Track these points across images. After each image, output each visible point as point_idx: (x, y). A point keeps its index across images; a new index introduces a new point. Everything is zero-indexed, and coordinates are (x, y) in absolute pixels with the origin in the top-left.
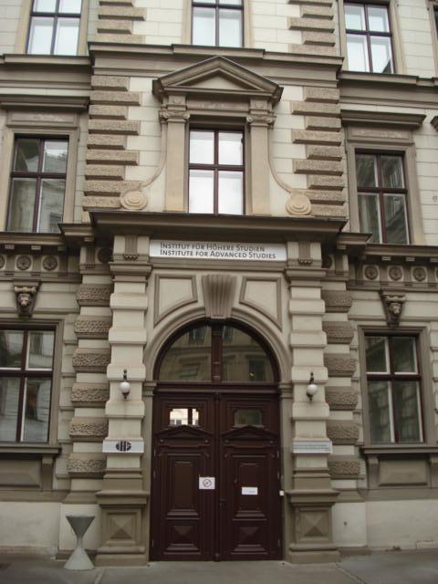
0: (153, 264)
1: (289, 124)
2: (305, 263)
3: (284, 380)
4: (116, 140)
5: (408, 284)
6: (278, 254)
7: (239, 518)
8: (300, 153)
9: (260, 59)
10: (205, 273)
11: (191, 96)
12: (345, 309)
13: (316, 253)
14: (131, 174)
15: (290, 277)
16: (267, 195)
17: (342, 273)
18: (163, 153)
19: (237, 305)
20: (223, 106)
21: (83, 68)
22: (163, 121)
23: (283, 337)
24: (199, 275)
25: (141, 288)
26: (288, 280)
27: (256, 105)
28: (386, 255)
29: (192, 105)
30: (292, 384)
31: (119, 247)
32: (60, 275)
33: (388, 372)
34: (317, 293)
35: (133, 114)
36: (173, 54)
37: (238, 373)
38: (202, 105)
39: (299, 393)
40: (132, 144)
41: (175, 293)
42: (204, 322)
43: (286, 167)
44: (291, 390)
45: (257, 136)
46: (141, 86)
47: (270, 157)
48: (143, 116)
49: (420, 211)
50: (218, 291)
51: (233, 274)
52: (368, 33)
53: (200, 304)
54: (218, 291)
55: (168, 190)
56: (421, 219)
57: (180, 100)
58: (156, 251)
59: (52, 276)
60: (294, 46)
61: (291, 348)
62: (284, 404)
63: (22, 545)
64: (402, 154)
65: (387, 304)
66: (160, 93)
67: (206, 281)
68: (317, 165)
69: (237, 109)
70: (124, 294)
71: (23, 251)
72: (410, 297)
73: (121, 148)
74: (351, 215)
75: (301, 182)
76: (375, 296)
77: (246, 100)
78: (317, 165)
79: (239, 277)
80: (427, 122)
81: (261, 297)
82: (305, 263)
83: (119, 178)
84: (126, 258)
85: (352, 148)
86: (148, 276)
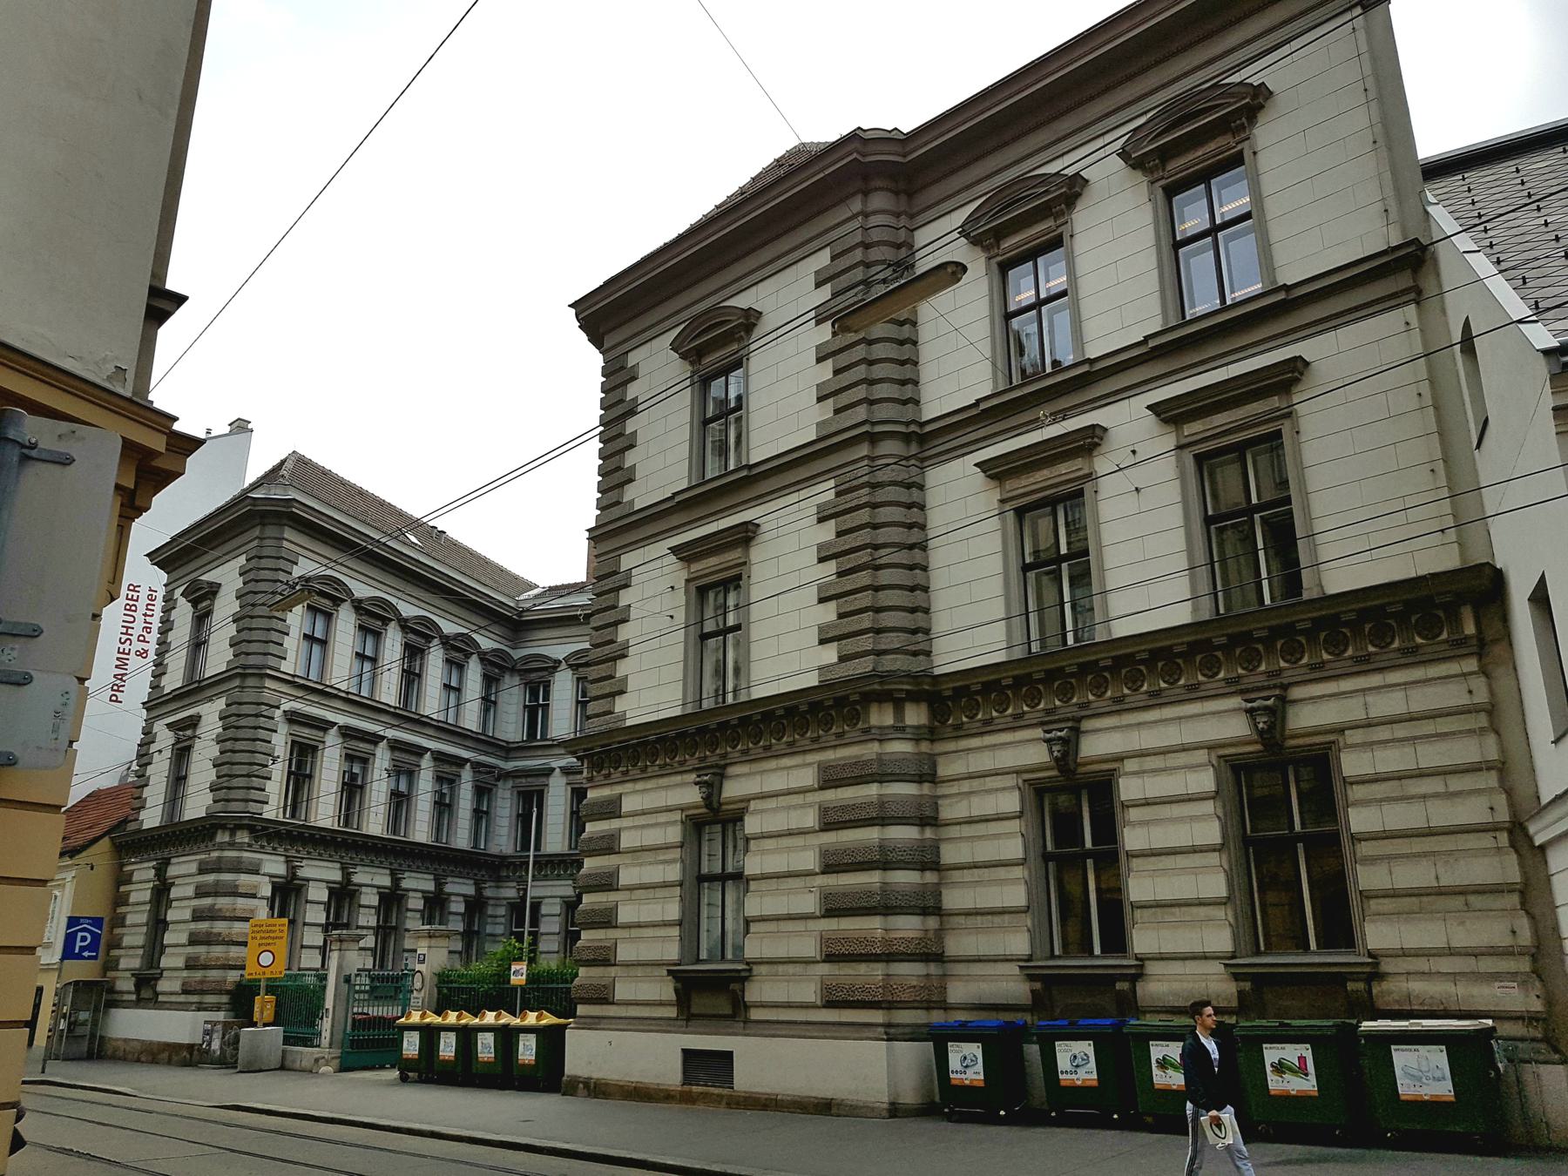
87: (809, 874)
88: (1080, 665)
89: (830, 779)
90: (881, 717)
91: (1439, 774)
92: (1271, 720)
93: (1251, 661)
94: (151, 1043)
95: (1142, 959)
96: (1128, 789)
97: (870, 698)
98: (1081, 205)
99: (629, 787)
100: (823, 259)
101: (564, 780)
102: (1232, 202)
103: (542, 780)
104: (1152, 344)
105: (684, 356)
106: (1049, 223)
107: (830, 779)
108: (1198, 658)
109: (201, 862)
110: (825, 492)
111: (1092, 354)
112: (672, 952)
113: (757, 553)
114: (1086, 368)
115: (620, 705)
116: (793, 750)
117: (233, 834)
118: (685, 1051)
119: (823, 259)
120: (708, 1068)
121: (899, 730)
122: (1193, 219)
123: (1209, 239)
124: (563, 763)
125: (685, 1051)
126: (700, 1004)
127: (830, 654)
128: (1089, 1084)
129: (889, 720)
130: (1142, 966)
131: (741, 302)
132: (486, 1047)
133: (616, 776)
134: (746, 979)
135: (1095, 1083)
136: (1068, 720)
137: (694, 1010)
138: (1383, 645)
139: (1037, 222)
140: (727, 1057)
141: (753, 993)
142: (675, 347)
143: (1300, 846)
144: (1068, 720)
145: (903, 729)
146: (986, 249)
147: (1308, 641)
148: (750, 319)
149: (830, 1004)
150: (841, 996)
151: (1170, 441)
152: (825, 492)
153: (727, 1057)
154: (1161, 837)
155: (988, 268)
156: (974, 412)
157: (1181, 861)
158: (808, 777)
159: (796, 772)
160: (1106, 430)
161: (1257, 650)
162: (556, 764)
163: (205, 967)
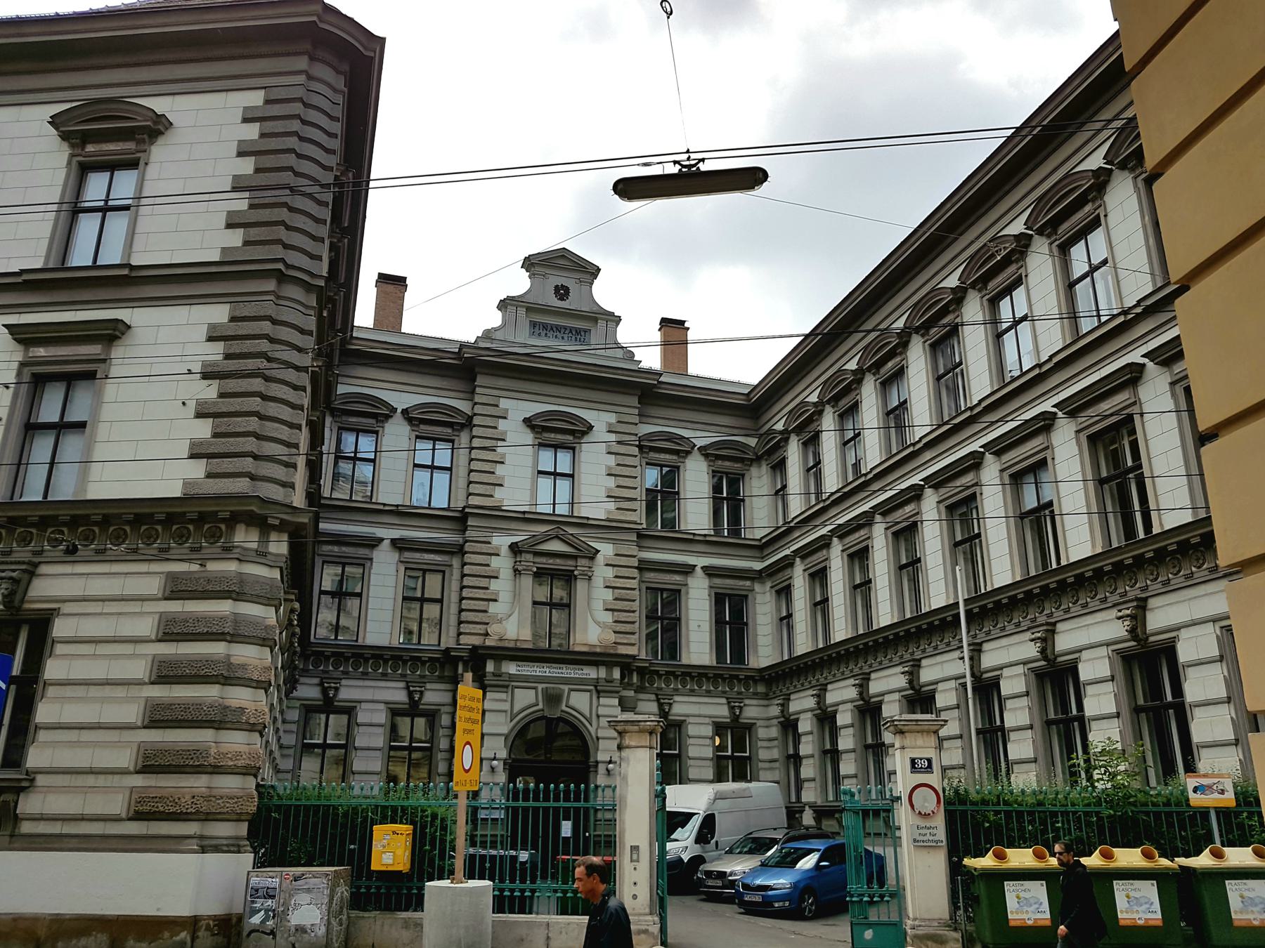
0: (512, 678)
1: (602, 573)
2: (609, 681)
3: (592, 759)
4: (483, 582)
5: (677, 690)
6: (591, 673)
7: (555, 762)
8: (609, 595)
9: (585, 524)
10: (544, 686)
11: (536, 554)
12: (632, 709)
13: (617, 674)
14: (493, 608)
15: (599, 690)
16: (585, 629)
17: (632, 685)
18: (516, 595)
19: (564, 708)
20: (558, 561)
21: (461, 519)
22: (517, 572)
23: (592, 730)
24: (540, 687)
25: (503, 696)
26: (598, 692)
27: (581, 562)
28: (662, 670)
29: (538, 560)
30: (597, 762)
31: (490, 667)
32: (439, 677)
33: (729, 753)
34: (616, 702)
35: (495, 562)
36: (526, 518)
37: (292, 845)
38: (544, 560)
39: (602, 768)
40: (494, 585)
41: (525, 698)
42: (543, 718)
43: (598, 606)
44: (596, 766)
45: (581, 586)
46: (502, 542)
47: (589, 599)
48: (502, 564)
49: (688, 635)
50: (553, 699)
51: (562, 686)
52: (555, 474)
53: (541, 706)
54: (553, 699)
55: (520, 624)
56: (688, 642)
57: (530, 557)
58: (512, 668)
59: (215, 550)
60: (609, 512)
61: (598, 739)
62: (592, 775)
63: (366, 914)
64: (679, 591)
65: (732, 708)
66: (515, 549)
67: (545, 691)
68: (620, 605)
69: (567, 565)
70: (495, 700)
71: (416, 661)
72: (677, 698)
73: (487, 588)
74: (636, 648)
75: (608, 618)
76: (653, 697)
77: (575, 557)
78: (620, 605)
79: (566, 688)
80: (698, 569)
81: (580, 701)
82: (609, 681)
83: (485, 611)
84: (494, 674)
85: (644, 586)
86: (507, 687)
87: (140, 683)
88: (73, 517)
89: (177, 590)
90: (246, 538)
91: (131, 642)
94: (35, 919)
95: (31, 777)
96: (60, 628)
97: (234, 520)
98: (161, 140)
100: (256, 99)
101: (395, 556)
102: (125, 185)
103: (362, 552)
105: (65, 136)
106: (130, 145)
107: (177, 590)
108: (206, 527)
109: (172, 577)
110: (219, 314)
111: (135, 261)
113: (117, 352)
114: (125, 272)
115: (499, 493)
116: (134, 555)
117: (264, 538)
119: (256, 99)
121: (261, 556)
122: (96, 188)
123: (110, 203)
124: (396, 534)
127: (197, 470)
128: (1151, 923)
130: (33, 780)
131: (159, 105)
134: (23, 789)
135: (1160, 923)
136: (24, 563)
138: (55, 543)
139: (118, 140)
142: (55, 121)
143: (1171, 711)
144: (24, 563)
146: (72, 146)
147: (163, 529)
148: (157, 127)
149: (138, 816)
152: (219, 314)
155: (69, 163)
156: (19, 280)
158: (153, 586)
159: (145, 578)
160: (129, 327)
161: (125, 531)
162: (388, 533)
163: (216, 770)
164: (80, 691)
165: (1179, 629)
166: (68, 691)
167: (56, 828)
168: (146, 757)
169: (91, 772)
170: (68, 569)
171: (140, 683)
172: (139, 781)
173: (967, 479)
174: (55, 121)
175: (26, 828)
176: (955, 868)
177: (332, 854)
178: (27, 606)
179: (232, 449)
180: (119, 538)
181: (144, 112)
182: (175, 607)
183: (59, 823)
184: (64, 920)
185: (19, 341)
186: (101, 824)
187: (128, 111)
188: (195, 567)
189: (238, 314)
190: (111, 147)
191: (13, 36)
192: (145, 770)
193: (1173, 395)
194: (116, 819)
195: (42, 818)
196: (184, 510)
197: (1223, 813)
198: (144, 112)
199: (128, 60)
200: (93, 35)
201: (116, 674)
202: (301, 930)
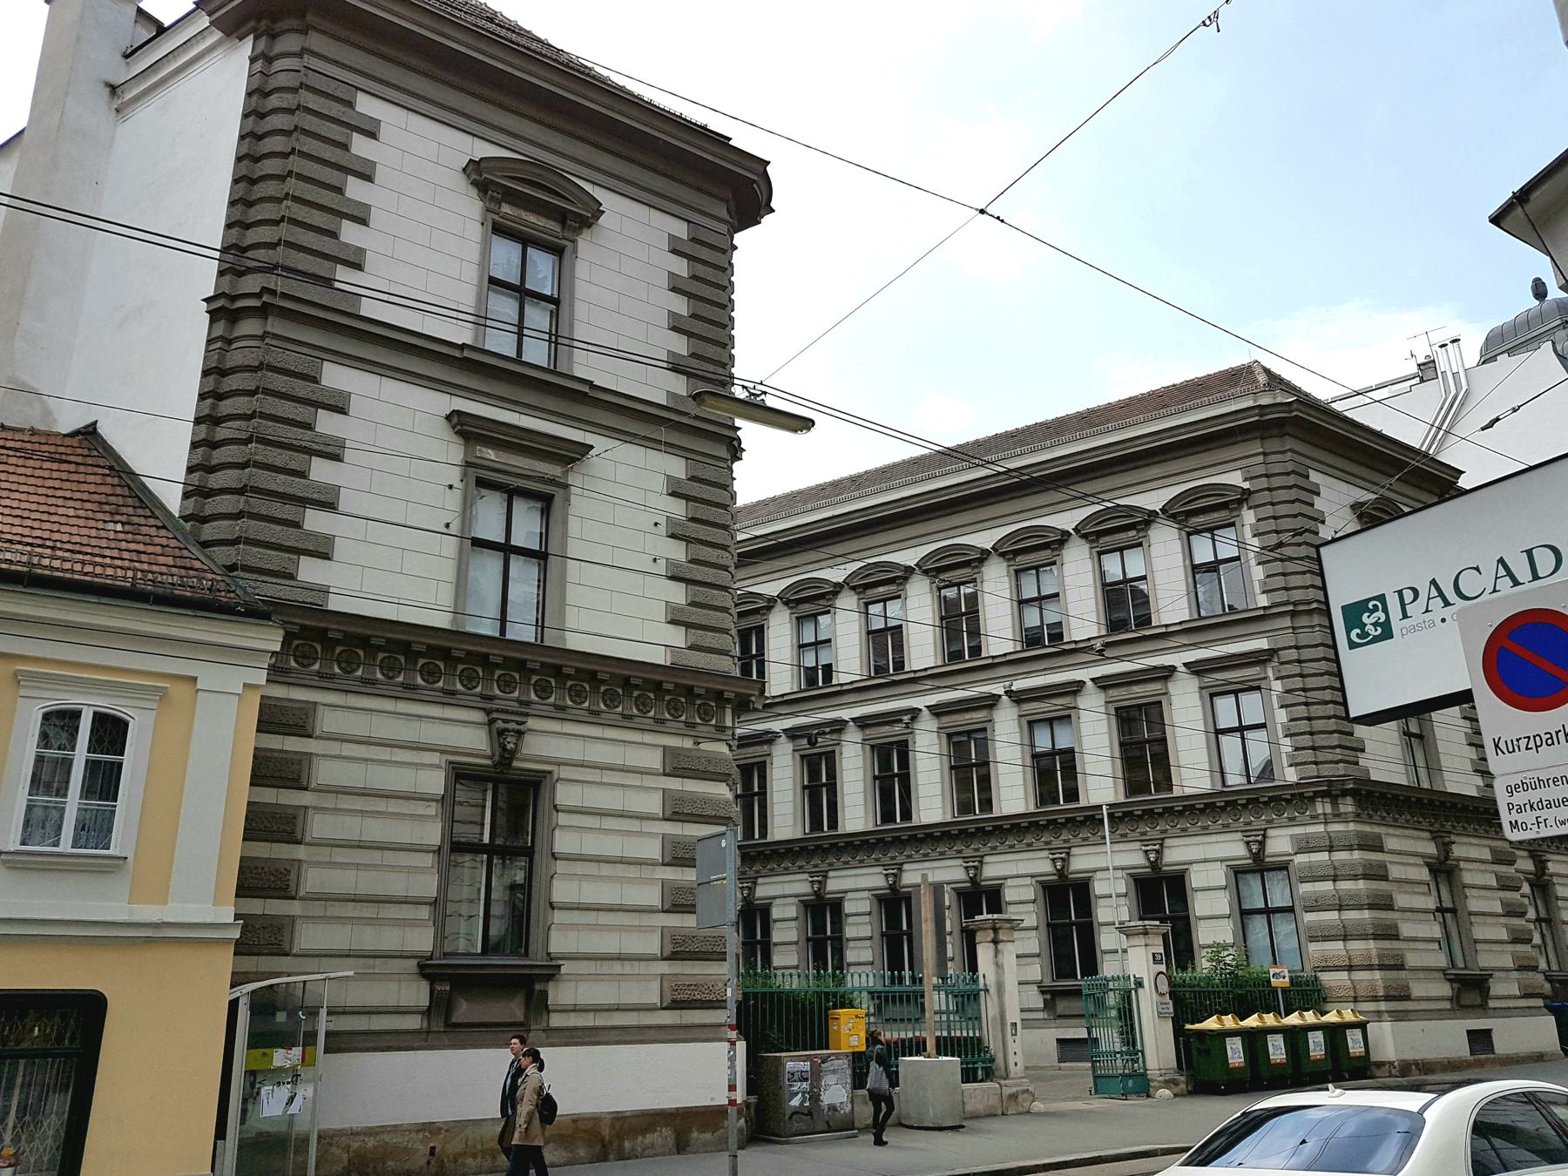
87: (652, 863)
89: (678, 766)
92: (505, 739)
93: (507, 685)
94: (596, 1119)
99: (1391, 831)
104: (467, 354)
107: (678, 766)
112: (422, 941)
117: (1335, 804)
118: (1469, 1032)
120: (1480, 1040)
121: (1338, 817)
125: (1469, 1032)
126: (1062, 1006)
129: (1329, 809)
132: (1277, 1050)
133: (1377, 818)
137: (1463, 1002)
138: (676, 717)
140: (1488, 1032)
141: (559, 994)
145: (1339, 815)
149: (676, 1005)
150: (1530, 991)
151: (573, 479)
153: (1488, 1032)
154: (593, 845)
156: (457, 354)
157: (606, 870)
164: (592, 868)
165: (1191, 863)
166: (579, 868)
167: (589, 1020)
168: (675, 942)
169: (620, 958)
170: (555, 726)
171: (653, 863)
172: (665, 968)
173: (980, 715)
174: (1355, 506)
175: (556, 1021)
176: (1178, 1032)
177: (804, 1042)
178: (515, 764)
179: (713, 623)
180: (611, 699)
181: (585, 198)
182: (674, 784)
183: (591, 1015)
184: (625, 1118)
185: (460, 433)
186: (364, 1018)
187: (572, 193)
188: (688, 743)
189: (699, 474)
190: (532, 218)
191: (496, 58)
192: (674, 957)
193: (1201, 697)
194: (1515, 997)
195: (576, 1009)
196: (370, 632)
197: (1284, 990)
198: (585, 198)
199: (549, 120)
200: (487, 60)
201: (630, 853)
202: (833, 1108)
